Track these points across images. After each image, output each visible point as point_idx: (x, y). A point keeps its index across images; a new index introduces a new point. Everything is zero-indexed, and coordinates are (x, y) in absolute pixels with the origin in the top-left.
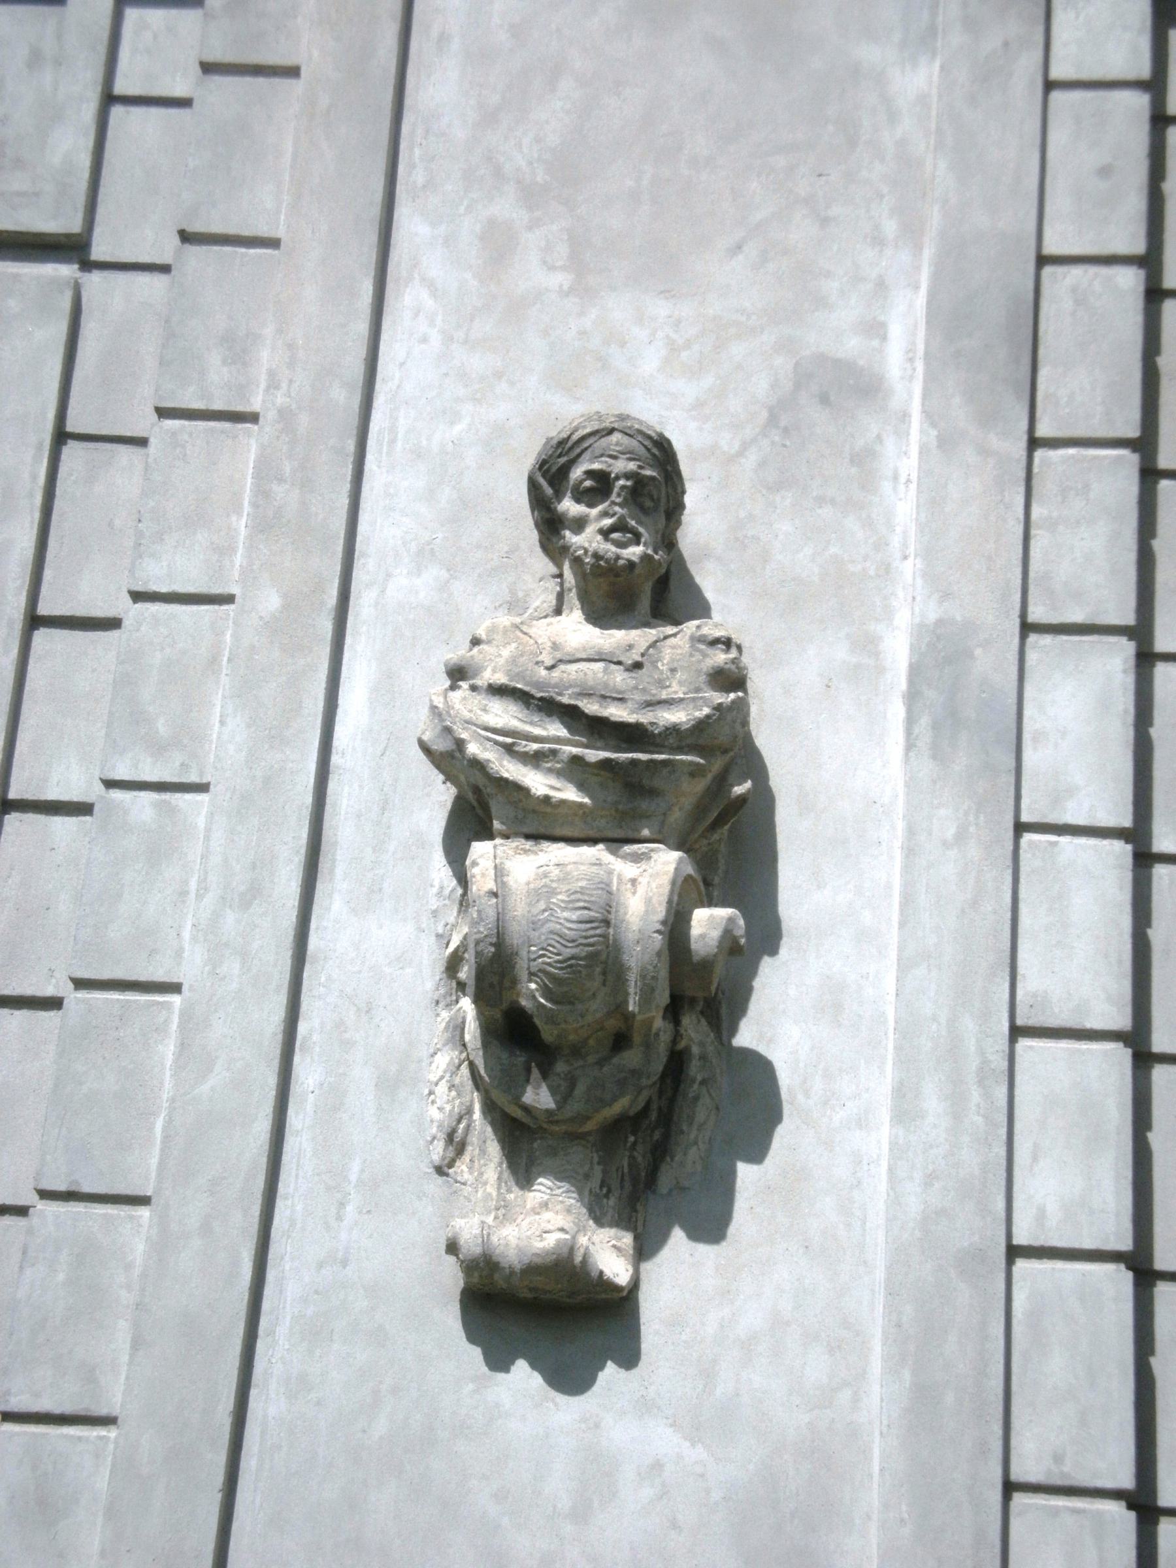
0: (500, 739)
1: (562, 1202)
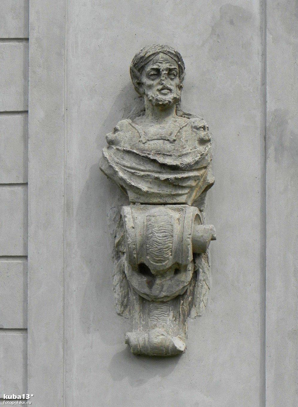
0: (130, 170)
1: (161, 324)
